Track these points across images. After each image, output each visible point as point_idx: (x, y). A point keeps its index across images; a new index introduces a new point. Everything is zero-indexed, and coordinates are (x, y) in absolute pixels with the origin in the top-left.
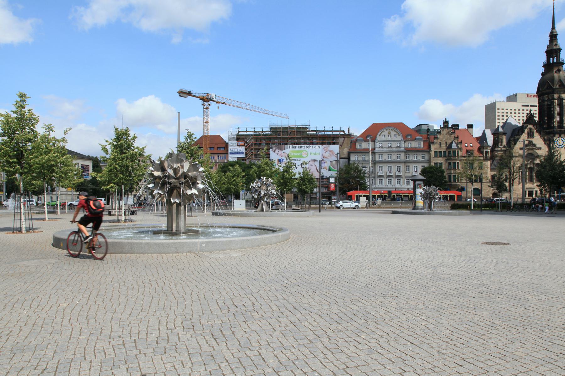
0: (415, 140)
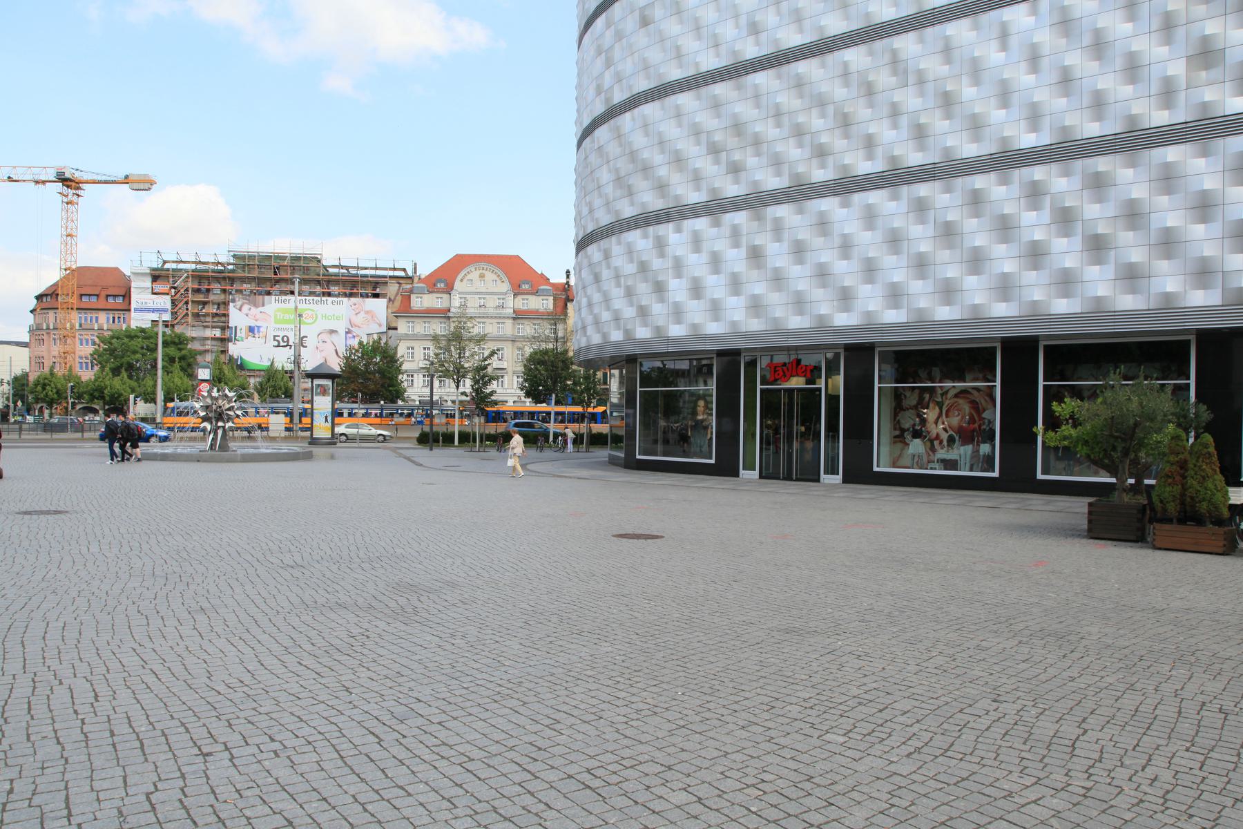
0: (535, 292)
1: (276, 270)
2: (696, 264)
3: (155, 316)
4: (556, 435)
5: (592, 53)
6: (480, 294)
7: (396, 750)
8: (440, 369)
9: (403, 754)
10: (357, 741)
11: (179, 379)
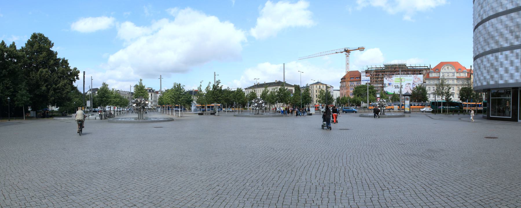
0: (463, 72)
1: (395, 68)
2: (507, 64)
3: (366, 82)
4: (468, 111)
5: (477, 4)
6: (447, 73)
7: (429, 193)
8: (438, 93)
9: (432, 194)
10: (420, 190)
11: (372, 97)
